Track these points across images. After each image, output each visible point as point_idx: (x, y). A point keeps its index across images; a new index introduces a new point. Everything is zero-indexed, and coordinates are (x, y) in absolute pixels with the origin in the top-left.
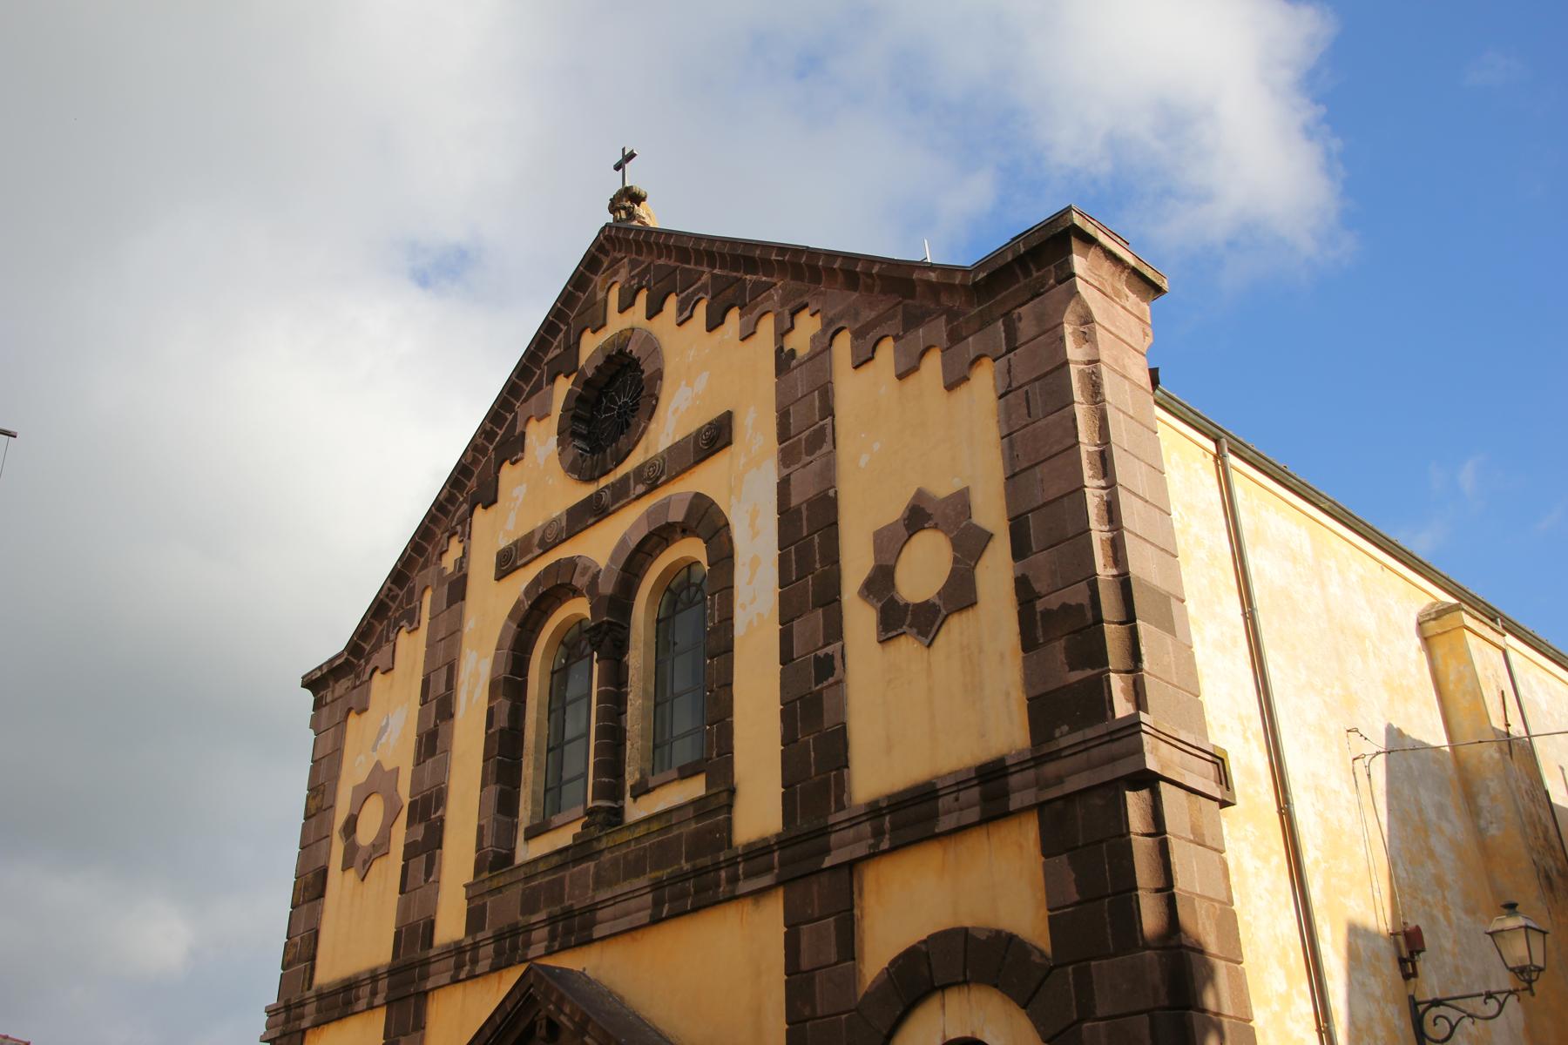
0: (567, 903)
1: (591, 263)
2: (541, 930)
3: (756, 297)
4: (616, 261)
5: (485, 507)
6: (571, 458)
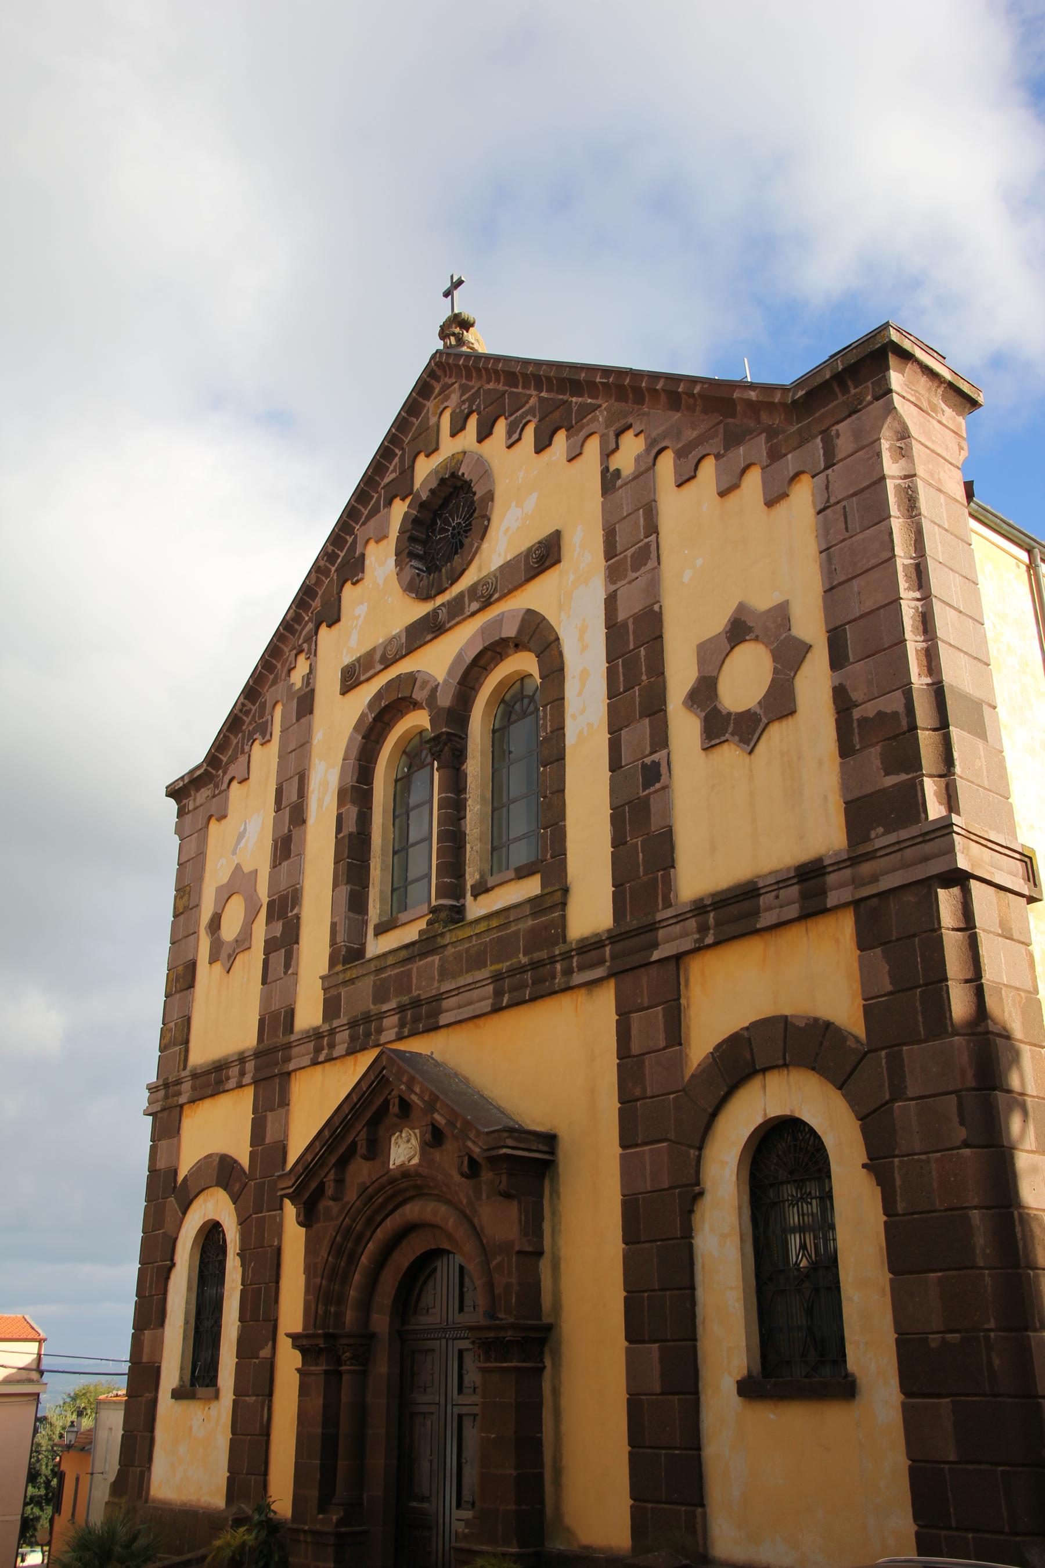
0: (415, 993)
1: (423, 389)
3: (582, 419)
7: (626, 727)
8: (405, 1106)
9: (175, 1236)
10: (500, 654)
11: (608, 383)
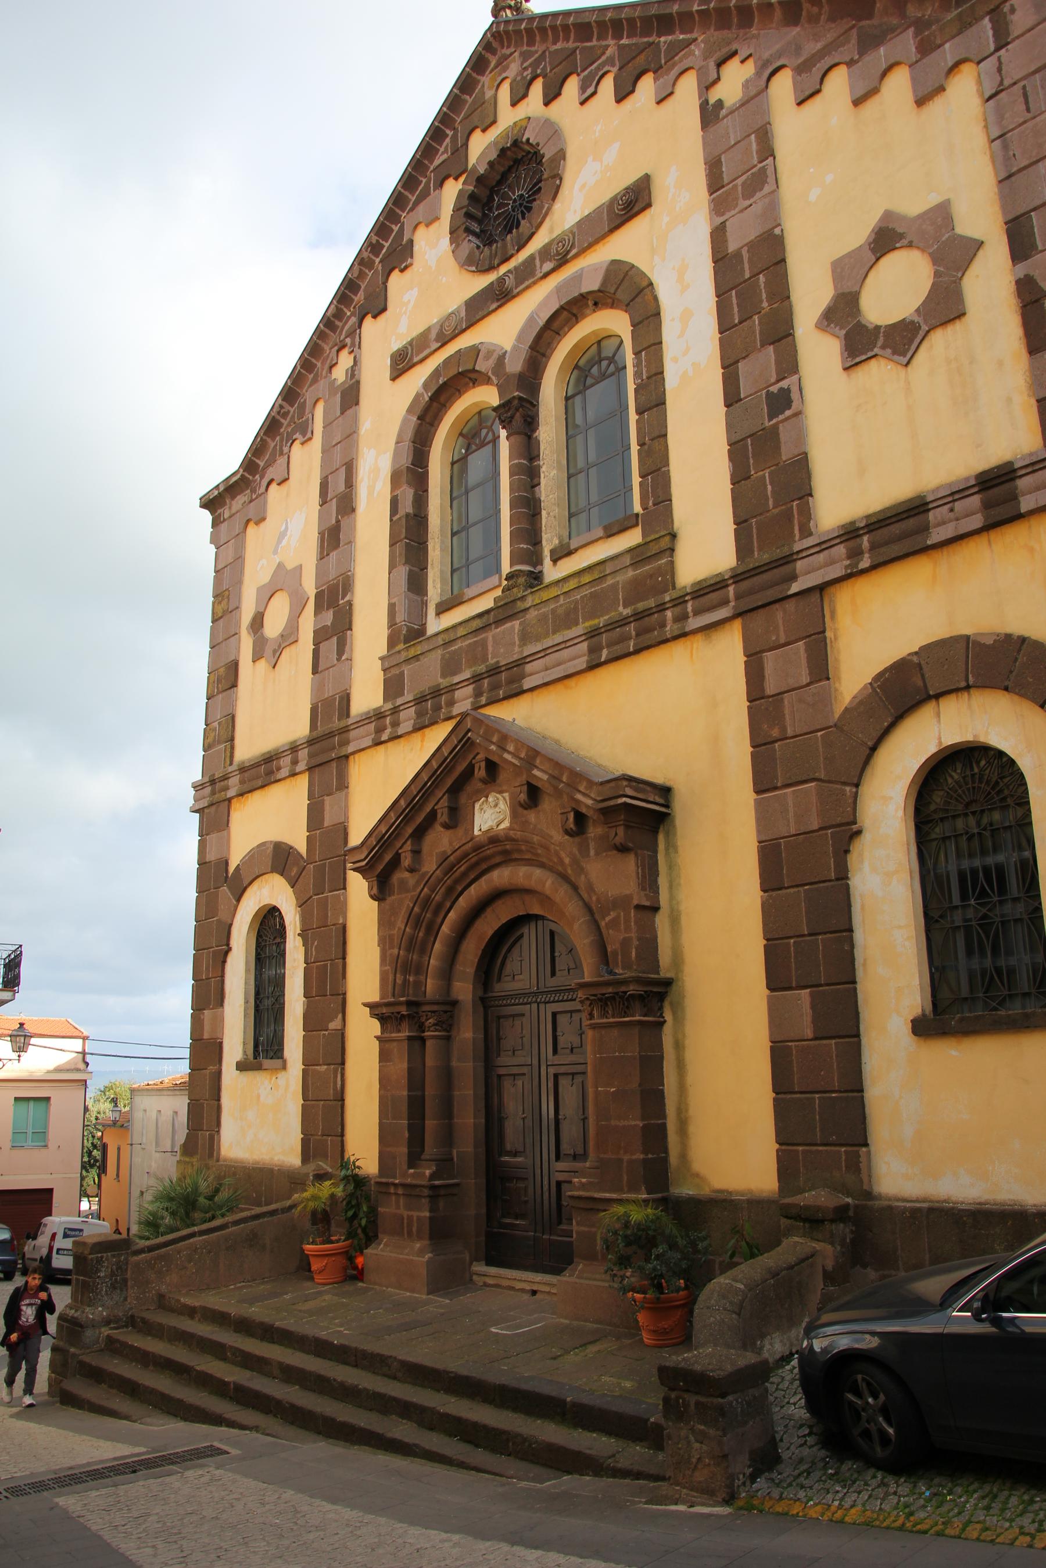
0: (492, 661)
1: (478, 63)
2: (466, 688)
3: (673, 58)
4: (506, 57)
5: (375, 317)
6: (467, 252)
7: (744, 358)
8: (492, 767)
9: (230, 922)
10: (575, 315)
11: (708, 10)
